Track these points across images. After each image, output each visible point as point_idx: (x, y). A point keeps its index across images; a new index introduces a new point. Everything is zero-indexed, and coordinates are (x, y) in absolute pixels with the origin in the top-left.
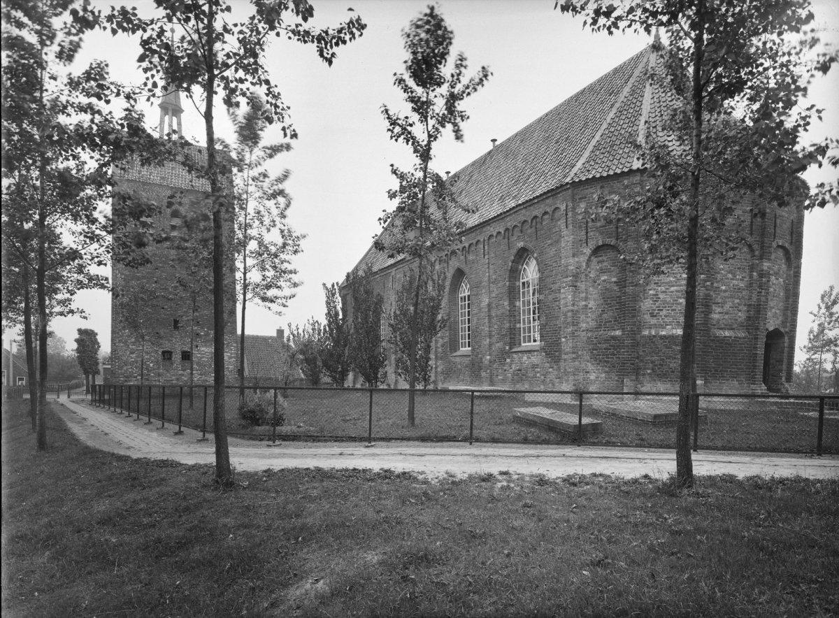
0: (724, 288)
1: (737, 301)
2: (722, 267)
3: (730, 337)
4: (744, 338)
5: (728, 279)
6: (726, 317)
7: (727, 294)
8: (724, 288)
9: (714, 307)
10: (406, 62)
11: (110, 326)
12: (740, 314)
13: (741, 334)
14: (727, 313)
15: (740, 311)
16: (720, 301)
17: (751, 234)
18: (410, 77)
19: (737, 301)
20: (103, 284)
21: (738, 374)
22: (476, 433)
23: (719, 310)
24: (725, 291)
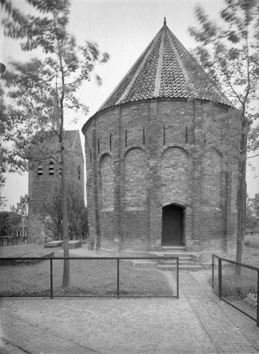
0: (131, 180)
1: (140, 188)
2: (129, 167)
3: (134, 211)
4: (144, 211)
5: (133, 174)
6: (135, 198)
7: (133, 184)
8: (131, 180)
9: (127, 193)
10: (43, 52)
11: (81, 138)
12: (143, 196)
13: (141, 209)
14: (135, 196)
15: (143, 194)
16: (130, 189)
17: (144, 144)
18: (19, 110)
19: (140, 188)
20: (10, 123)
21: (140, 235)
22: (122, 288)
23: (130, 194)
24: (132, 182)
